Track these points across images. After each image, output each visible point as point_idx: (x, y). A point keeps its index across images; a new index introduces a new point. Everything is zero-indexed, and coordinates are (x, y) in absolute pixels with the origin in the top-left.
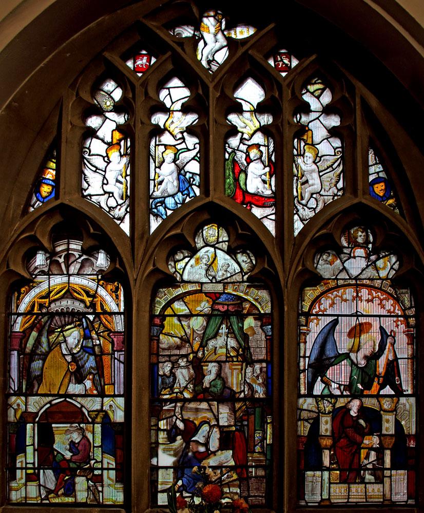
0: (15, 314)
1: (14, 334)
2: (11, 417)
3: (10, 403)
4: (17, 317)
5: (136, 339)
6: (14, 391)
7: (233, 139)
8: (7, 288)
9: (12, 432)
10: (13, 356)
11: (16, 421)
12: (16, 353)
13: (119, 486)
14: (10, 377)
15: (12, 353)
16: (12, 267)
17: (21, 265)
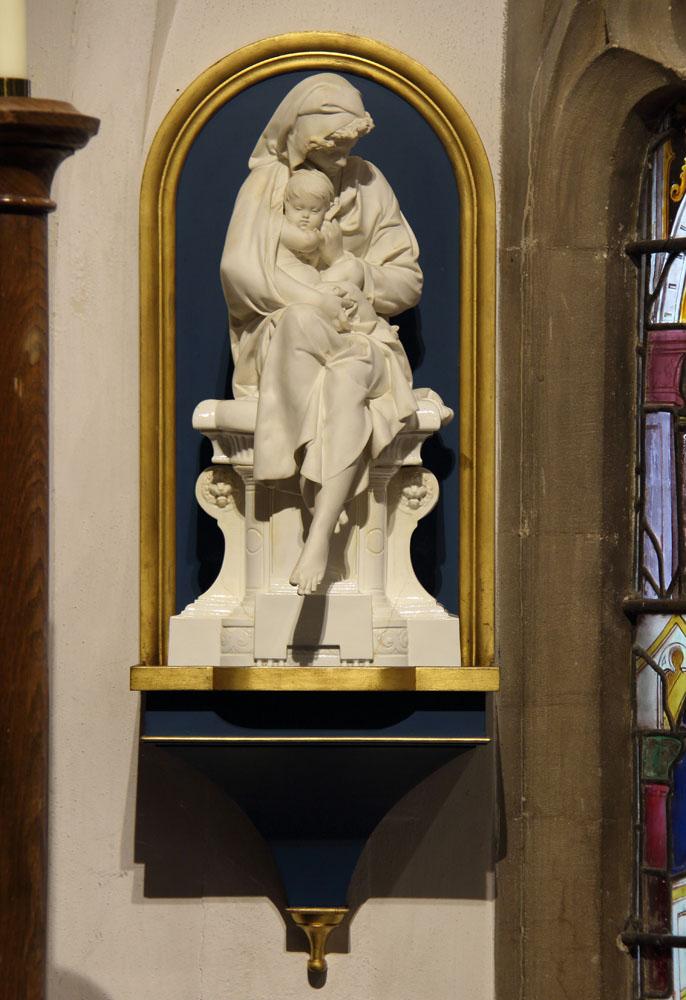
0: (659, 247)
1: (654, 334)
2: (647, 709)
3: (644, 647)
4: (670, 261)
5: (504, 333)
6: (660, 591)
7: (392, 52)
8: (615, 136)
9: (651, 774)
10: (655, 435)
11: (667, 727)
12: (664, 421)
13: (406, 612)
14: (644, 528)
15: (651, 419)
16: (624, 40)
17: (668, 20)
